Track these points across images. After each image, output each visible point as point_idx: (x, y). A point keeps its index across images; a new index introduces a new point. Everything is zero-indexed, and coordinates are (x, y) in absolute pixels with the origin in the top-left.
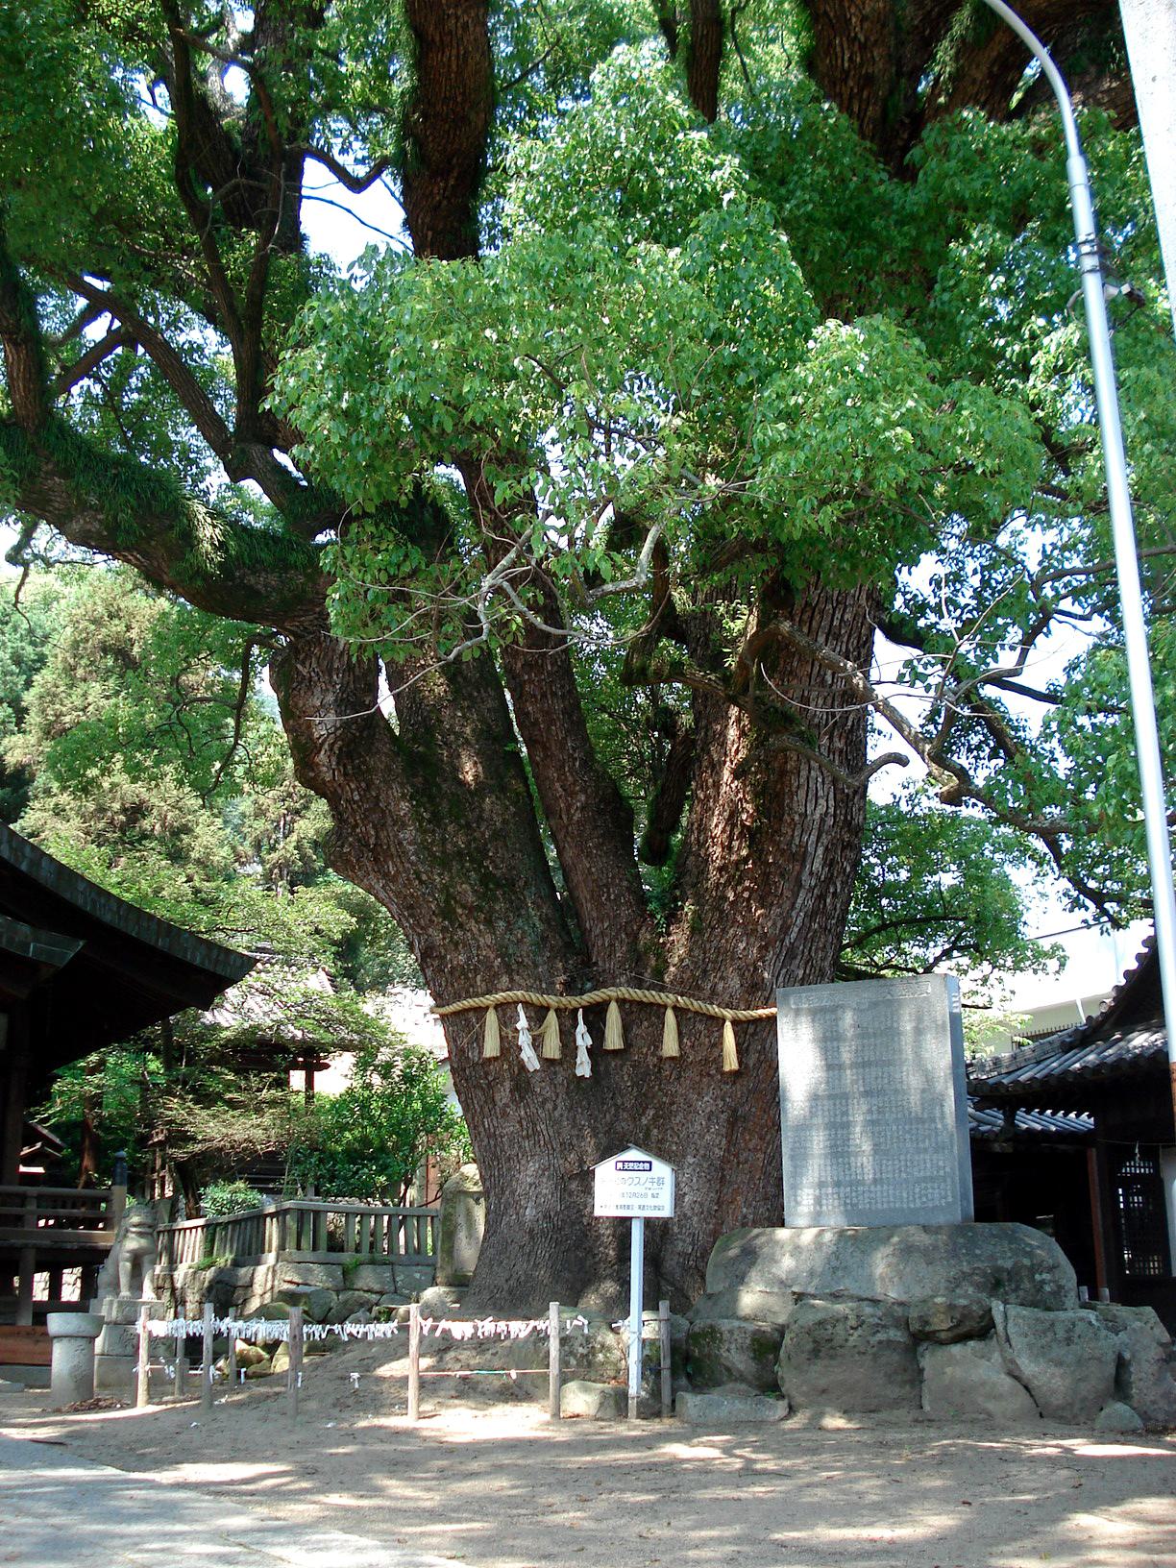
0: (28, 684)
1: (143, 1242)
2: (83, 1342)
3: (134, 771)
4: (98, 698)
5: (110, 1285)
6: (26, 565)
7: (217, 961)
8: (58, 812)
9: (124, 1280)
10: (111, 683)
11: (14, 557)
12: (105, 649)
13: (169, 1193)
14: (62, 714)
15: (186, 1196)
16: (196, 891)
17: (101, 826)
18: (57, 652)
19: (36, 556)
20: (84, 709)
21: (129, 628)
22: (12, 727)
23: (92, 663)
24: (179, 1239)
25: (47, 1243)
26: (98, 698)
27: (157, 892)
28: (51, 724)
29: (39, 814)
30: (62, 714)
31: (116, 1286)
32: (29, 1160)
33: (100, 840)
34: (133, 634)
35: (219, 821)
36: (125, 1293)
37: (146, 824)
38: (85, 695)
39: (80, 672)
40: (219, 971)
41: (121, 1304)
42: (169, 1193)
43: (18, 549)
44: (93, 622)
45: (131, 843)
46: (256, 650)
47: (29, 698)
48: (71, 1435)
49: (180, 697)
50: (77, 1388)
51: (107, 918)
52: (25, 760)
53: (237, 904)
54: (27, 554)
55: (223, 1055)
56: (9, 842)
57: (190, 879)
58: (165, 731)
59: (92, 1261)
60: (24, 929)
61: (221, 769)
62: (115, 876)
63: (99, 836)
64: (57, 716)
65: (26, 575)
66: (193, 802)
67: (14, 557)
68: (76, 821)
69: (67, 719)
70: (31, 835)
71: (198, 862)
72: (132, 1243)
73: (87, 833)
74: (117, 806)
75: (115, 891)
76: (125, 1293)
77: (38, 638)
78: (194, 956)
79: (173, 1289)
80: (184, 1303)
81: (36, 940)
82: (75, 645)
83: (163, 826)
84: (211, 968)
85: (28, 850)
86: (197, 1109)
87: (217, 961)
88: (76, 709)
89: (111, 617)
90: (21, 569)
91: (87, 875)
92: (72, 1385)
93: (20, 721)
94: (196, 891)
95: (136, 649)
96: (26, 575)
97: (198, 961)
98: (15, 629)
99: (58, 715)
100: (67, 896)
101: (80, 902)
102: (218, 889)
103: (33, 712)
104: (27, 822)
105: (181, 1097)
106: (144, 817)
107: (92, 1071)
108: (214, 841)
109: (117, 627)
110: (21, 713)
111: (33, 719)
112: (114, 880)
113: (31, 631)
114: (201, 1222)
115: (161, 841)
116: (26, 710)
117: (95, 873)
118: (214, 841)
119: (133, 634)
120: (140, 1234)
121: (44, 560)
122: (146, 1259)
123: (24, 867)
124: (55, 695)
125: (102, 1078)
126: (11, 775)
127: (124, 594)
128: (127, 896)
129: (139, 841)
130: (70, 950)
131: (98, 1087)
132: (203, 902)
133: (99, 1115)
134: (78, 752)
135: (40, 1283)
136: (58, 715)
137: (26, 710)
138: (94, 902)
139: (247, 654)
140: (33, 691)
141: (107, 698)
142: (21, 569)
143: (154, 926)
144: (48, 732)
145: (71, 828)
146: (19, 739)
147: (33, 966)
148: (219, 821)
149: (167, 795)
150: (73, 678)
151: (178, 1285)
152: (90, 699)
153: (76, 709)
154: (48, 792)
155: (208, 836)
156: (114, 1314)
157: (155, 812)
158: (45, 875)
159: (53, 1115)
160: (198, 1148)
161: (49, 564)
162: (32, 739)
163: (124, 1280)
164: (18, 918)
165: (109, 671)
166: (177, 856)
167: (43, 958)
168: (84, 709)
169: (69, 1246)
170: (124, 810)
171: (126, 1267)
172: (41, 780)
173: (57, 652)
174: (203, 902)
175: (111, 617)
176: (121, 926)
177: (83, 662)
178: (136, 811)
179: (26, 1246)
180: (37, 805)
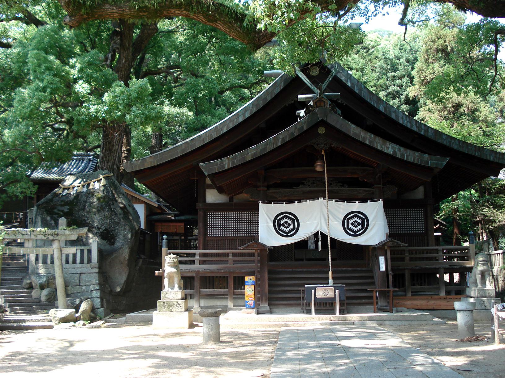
0: (413, 68)
1: (485, 267)
2: (468, 313)
3: (458, 91)
4: (438, 68)
5: (473, 283)
6: (406, 25)
7: (499, 158)
8: (430, 110)
9: (479, 281)
10: (442, 62)
11: (401, 23)
12: (438, 51)
13: (485, 238)
14: (426, 76)
15: (493, 241)
16: (484, 132)
17: (446, 113)
18: (421, 55)
19: (409, 21)
20: (434, 73)
21: (445, 41)
22: (409, 84)
23: (434, 56)
24: (493, 258)
25: (447, 266)
26: (438, 68)
27: (469, 134)
28: (423, 80)
29: (423, 113)
30: (426, 76)
31: (475, 283)
32: (436, 231)
33: (446, 118)
34: (447, 43)
35: (488, 105)
36: (479, 286)
37: (462, 110)
38: (433, 68)
39: (430, 60)
40: (501, 162)
41: (478, 290)
42: (485, 238)
43: (402, 19)
44: (432, 41)
45: (457, 118)
46: (499, 36)
47: (414, 73)
48: (473, 363)
49: (468, 61)
50: (468, 330)
51: (456, 147)
52: (416, 95)
53: (501, 135)
54: (405, 21)
55: (501, 190)
56: (416, 125)
57: (481, 128)
58: (467, 74)
59: (464, 271)
60: (426, 156)
61: (491, 85)
62: (453, 130)
63: (445, 117)
64: (425, 77)
65: (406, 29)
66: (478, 98)
67: (401, 23)
68: (437, 113)
69: (428, 78)
70: (421, 120)
71: (483, 121)
72: (481, 268)
73: (441, 117)
74: (450, 105)
75: (454, 136)
76: (479, 286)
77: (413, 51)
78: (490, 157)
79: (493, 276)
80: (497, 280)
81: (431, 160)
82: (427, 51)
83: (468, 110)
84: (497, 161)
85: (423, 127)
86: (495, 211)
87: (499, 158)
88: (431, 74)
89: (438, 39)
90: (404, 27)
91: (444, 131)
92: (466, 329)
93: (412, 82)
94: (484, 132)
95: (449, 48)
96: (406, 29)
97: (492, 159)
98: (405, 51)
99: (425, 77)
100: (440, 141)
101: (445, 143)
102: (492, 130)
103: (416, 77)
104: (106, 93)
105: (488, 207)
106: (461, 108)
107: (454, 200)
108: (487, 112)
109: (441, 42)
110: (412, 79)
111: (416, 80)
112: (453, 132)
113: (411, 49)
114: (501, 251)
115: (468, 115)
116: (413, 77)
117: (446, 131)
118: (487, 112)
119: (447, 43)
120: (483, 264)
121: (412, 22)
122: (486, 273)
123: (422, 133)
124: (423, 70)
125: (457, 202)
126: (412, 101)
127: (441, 29)
128: (459, 137)
129: (460, 117)
130: (442, 162)
131: (457, 205)
132: (488, 136)
133: (459, 216)
134: (434, 88)
135: (447, 277)
136: (425, 77)
137: (413, 77)
138: (450, 142)
139: (496, 38)
140: (415, 70)
141: (441, 67)
142: (404, 27)
143: (473, 149)
144: (422, 84)
145: (435, 116)
146: (412, 88)
147: (431, 169)
148: (488, 105)
149: (469, 98)
150: (428, 63)
151: (495, 274)
152: (435, 69)
153: (431, 74)
154: (425, 104)
155: (485, 111)
156: (476, 294)
157: (464, 105)
158: (430, 135)
159: (442, 216)
160: (496, 225)
161: (414, 23)
162: (417, 87)
163: (479, 281)
164: (424, 152)
165: (440, 58)
166: (474, 120)
167: (435, 166)
168: (434, 73)
169: (456, 267)
170: (453, 106)
171: (479, 277)
172: (422, 101)
173: (421, 55)
174: (488, 136)
175: (438, 39)
176: (461, 150)
177: (431, 57)
178: (458, 106)
179: (440, 268)
180: (422, 109)
